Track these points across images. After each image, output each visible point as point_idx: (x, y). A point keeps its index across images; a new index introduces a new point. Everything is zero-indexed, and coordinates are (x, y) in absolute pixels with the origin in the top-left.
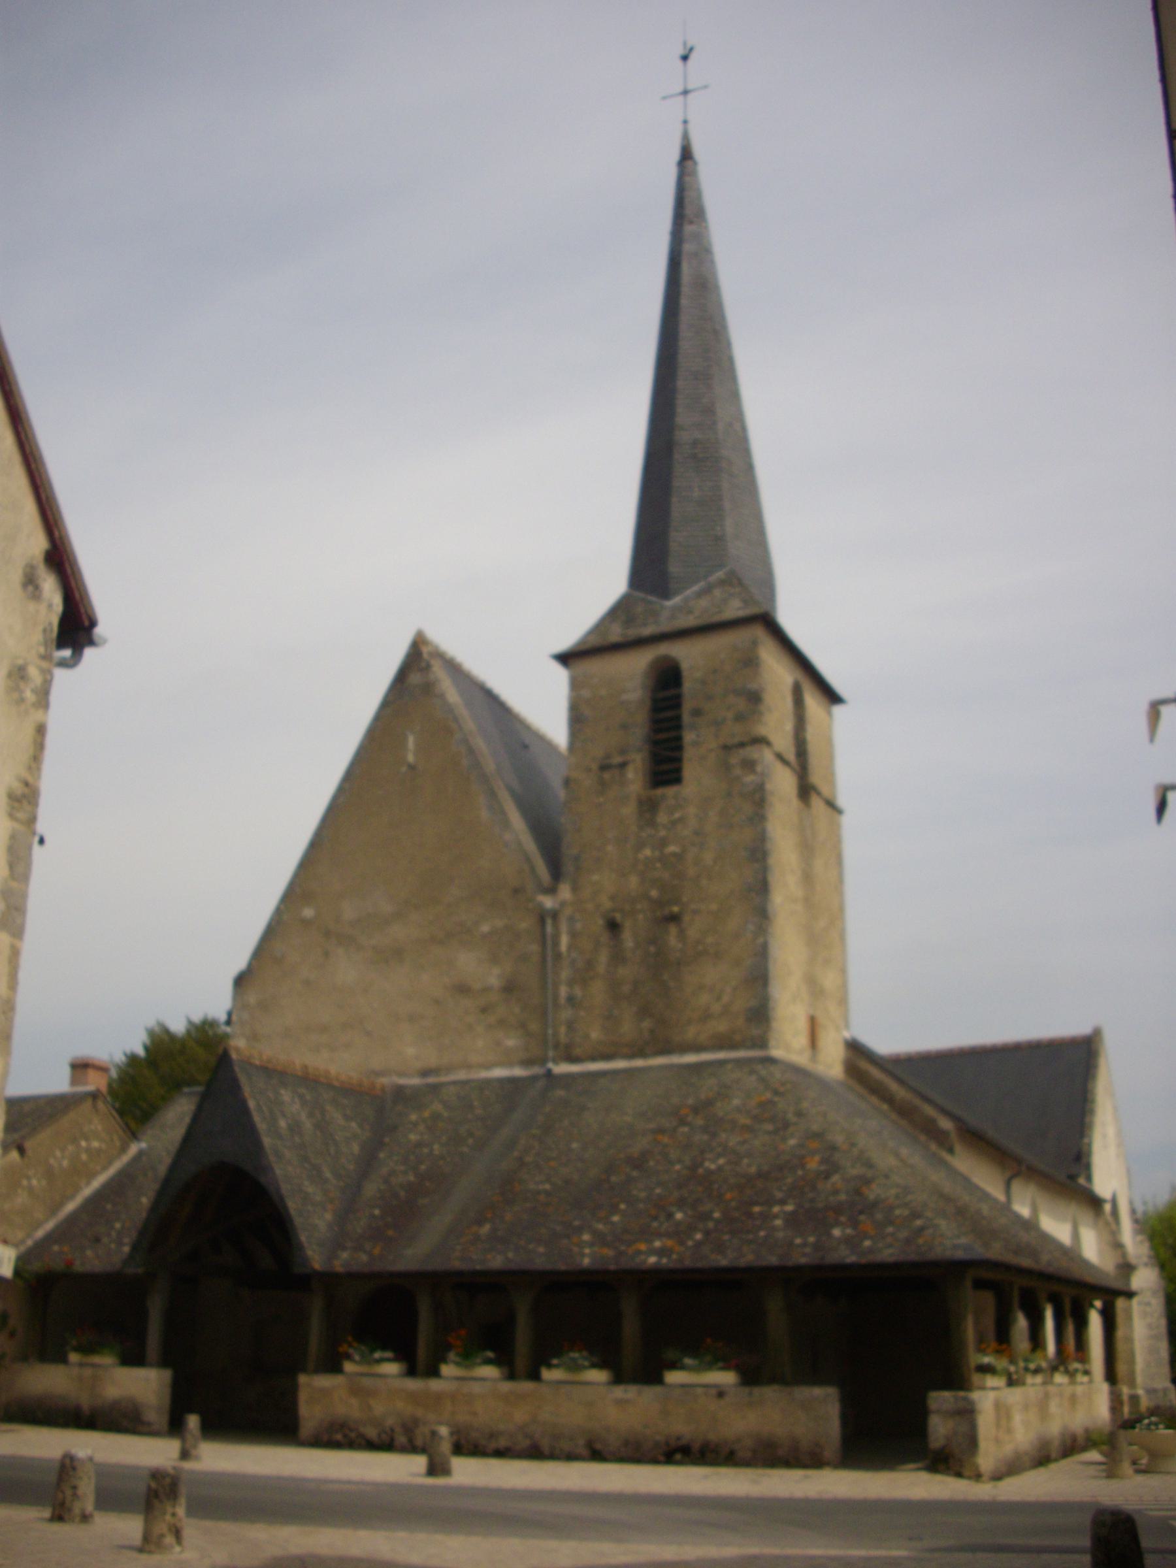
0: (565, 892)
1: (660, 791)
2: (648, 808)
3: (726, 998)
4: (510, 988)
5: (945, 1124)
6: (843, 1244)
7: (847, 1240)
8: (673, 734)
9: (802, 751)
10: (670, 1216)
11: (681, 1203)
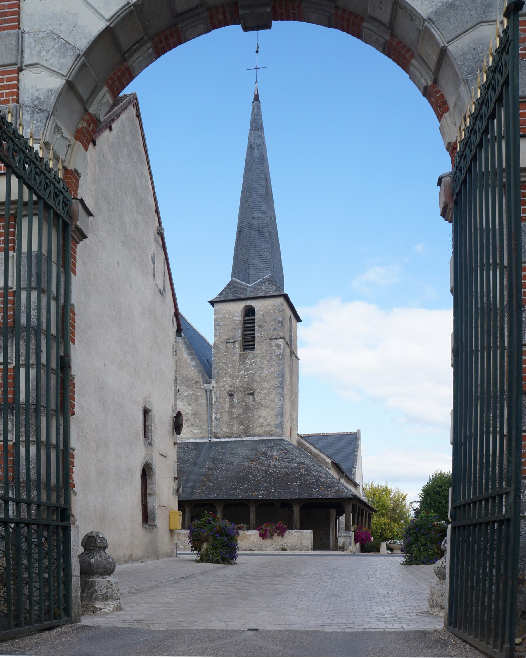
0: (214, 383)
1: (247, 352)
2: (243, 358)
3: (268, 421)
5: (329, 461)
6: (316, 493)
7: (318, 492)
10: (263, 485)
11: (265, 481)
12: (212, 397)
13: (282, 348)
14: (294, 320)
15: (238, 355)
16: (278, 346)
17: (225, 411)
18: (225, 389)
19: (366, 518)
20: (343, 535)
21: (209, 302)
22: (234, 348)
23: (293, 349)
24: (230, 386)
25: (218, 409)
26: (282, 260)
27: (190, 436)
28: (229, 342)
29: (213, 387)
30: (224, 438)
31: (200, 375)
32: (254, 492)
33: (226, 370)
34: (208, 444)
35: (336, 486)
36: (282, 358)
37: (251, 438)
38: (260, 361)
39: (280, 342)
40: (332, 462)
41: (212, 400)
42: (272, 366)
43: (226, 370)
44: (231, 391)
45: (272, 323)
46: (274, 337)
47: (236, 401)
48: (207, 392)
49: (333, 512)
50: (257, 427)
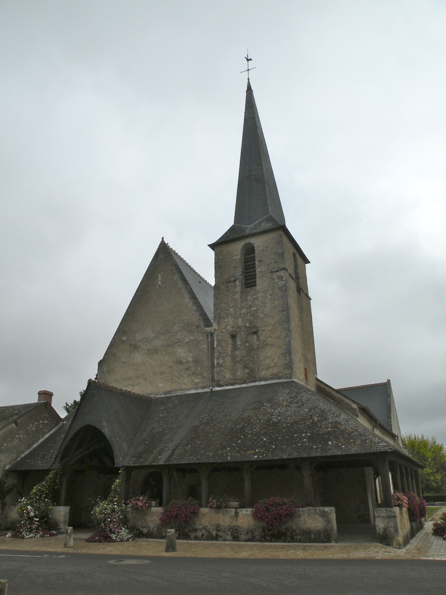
3: (275, 361)
4: (196, 361)
5: (355, 406)
6: (335, 449)
8: (253, 262)
9: (296, 273)
10: (262, 440)
11: (265, 435)
12: (213, 341)
13: (284, 279)
14: (299, 260)
15: (239, 293)
16: (280, 278)
17: (228, 355)
18: (227, 331)
19: (412, 479)
20: (383, 514)
21: (210, 246)
22: (235, 287)
23: (301, 286)
24: (233, 327)
25: (220, 353)
26: (282, 204)
27: (191, 386)
28: (230, 282)
29: (215, 330)
30: (227, 385)
31: (201, 318)
32: (248, 450)
33: (227, 310)
34: (208, 394)
35: (360, 434)
36: (286, 289)
37: (257, 383)
38: (262, 297)
39: (282, 273)
40: (360, 408)
41: (214, 344)
42: (275, 299)
43: (227, 310)
44: (233, 332)
45: (272, 257)
46: (275, 270)
47: (239, 343)
48: (208, 336)
49: (369, 471)
50: (263, 369)
